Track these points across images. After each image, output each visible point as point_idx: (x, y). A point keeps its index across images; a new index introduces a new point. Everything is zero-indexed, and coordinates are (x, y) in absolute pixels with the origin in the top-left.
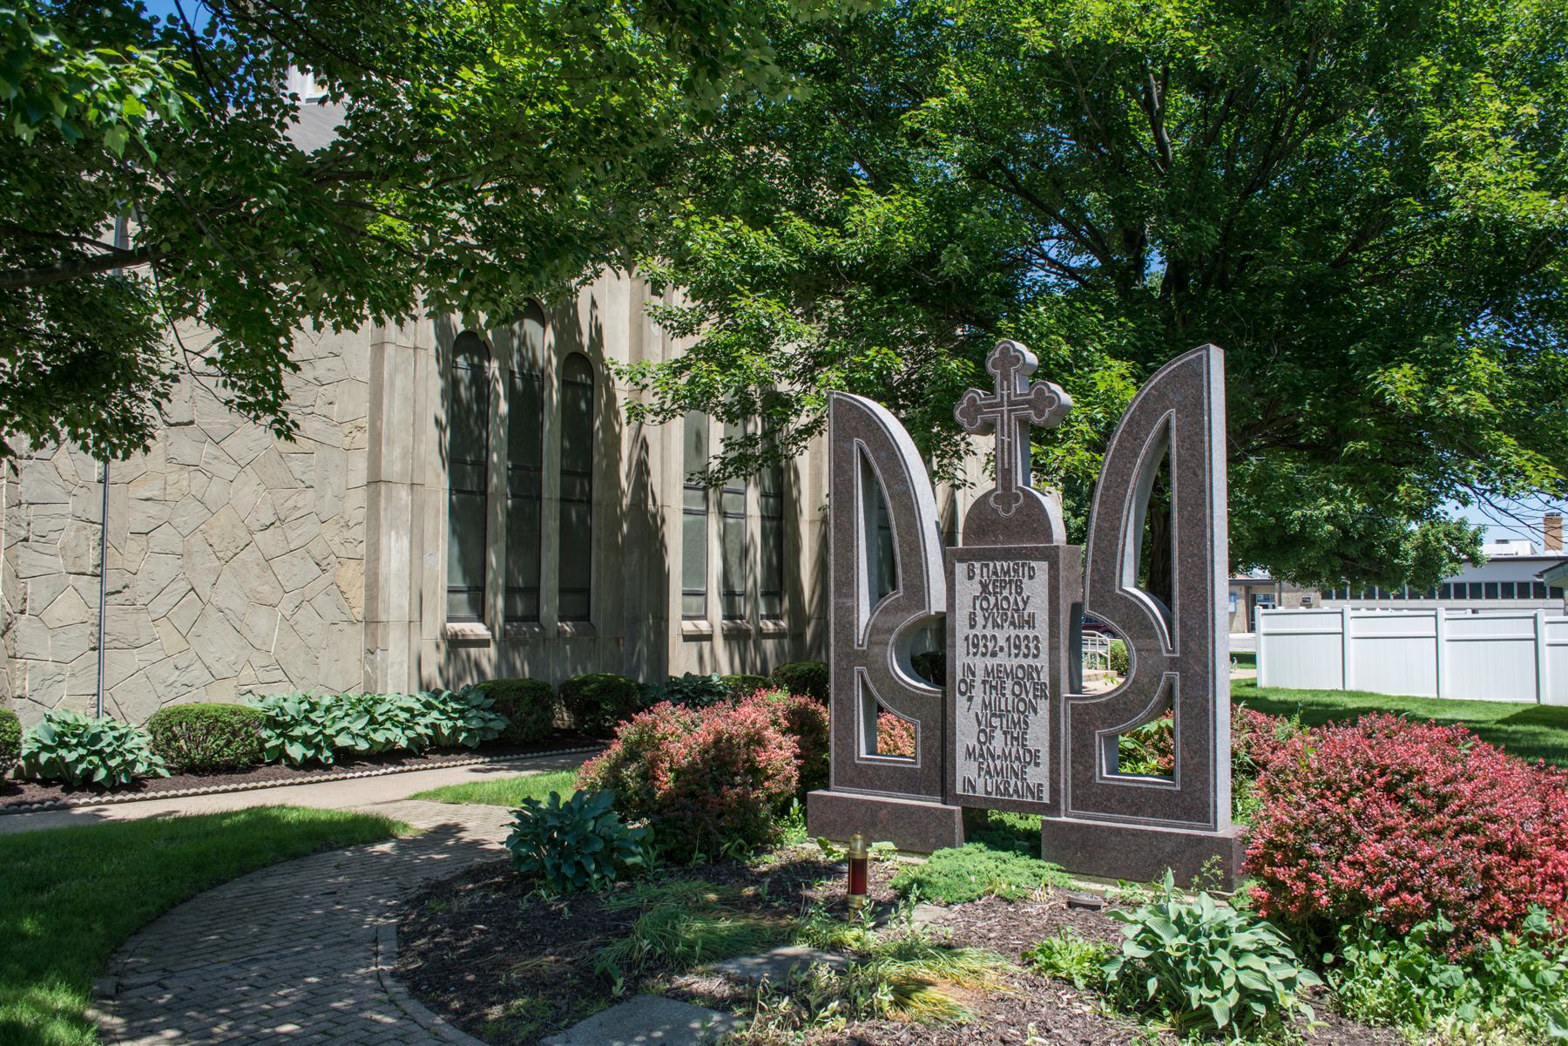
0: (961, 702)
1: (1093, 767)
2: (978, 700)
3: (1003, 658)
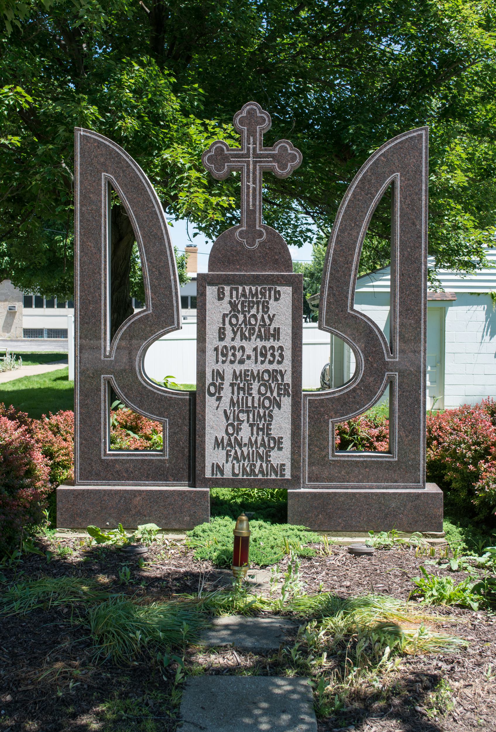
3: (250, 365)
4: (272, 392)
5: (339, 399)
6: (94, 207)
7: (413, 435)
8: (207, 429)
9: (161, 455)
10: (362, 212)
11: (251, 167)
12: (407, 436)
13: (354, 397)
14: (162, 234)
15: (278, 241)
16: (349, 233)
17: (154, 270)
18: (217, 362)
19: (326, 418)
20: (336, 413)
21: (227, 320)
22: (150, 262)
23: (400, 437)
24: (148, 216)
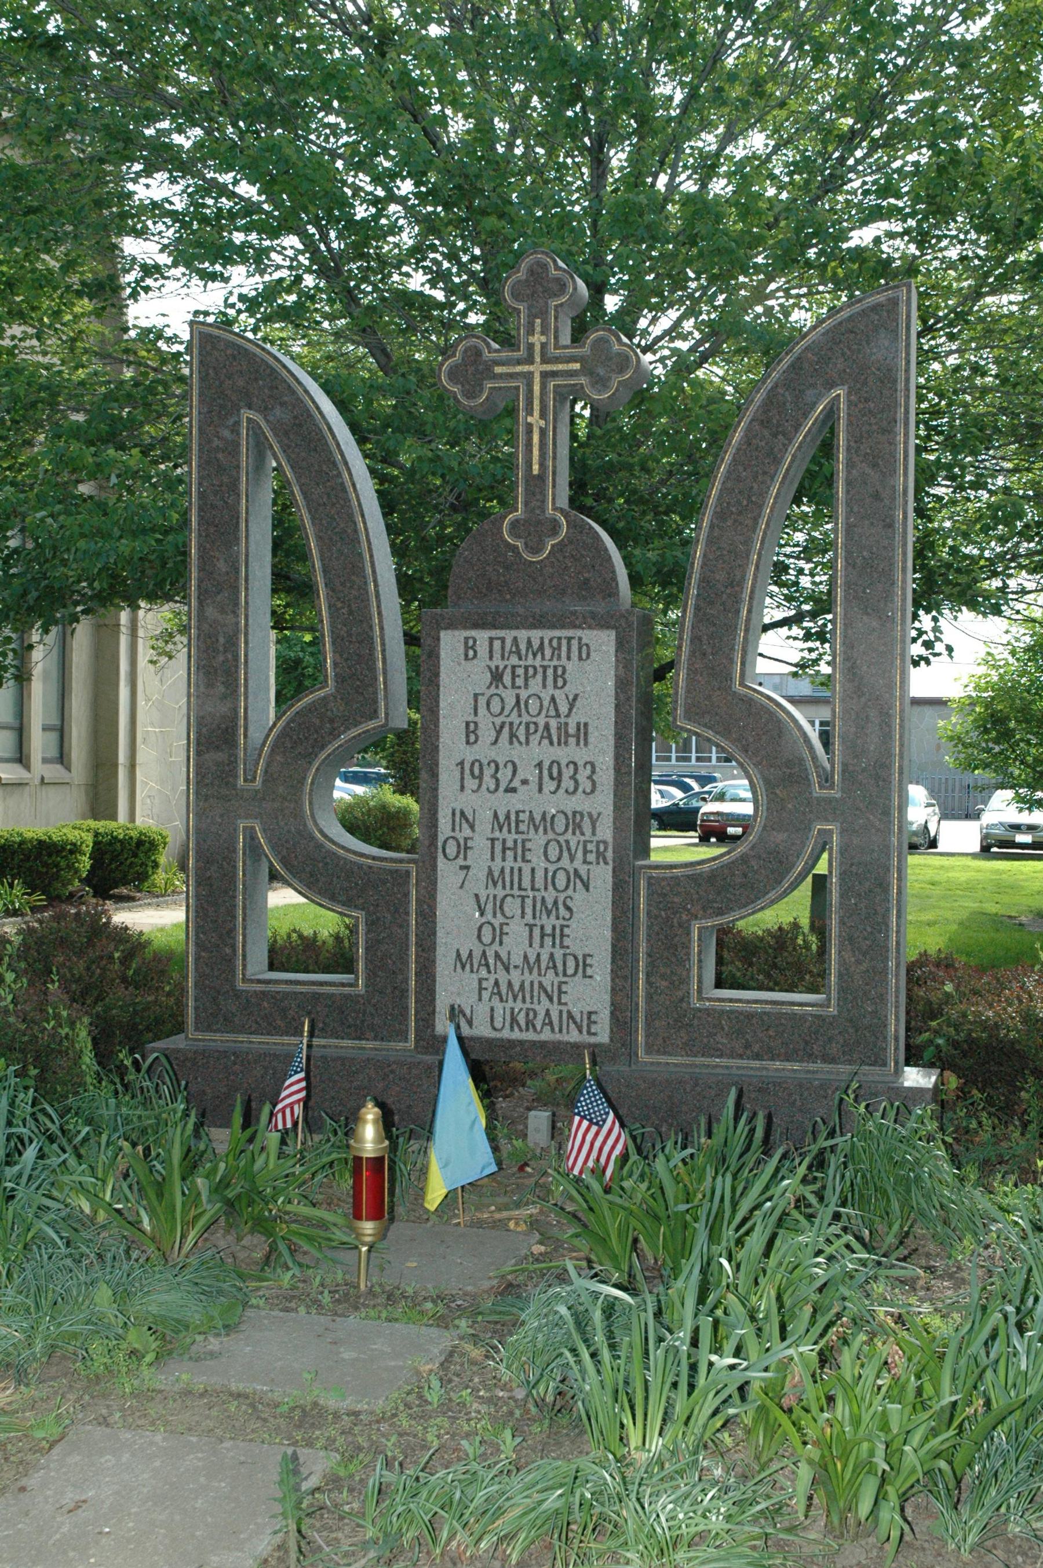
0: (447, 872)
1: (685, 981)
2: (479, 872)
3: (525, 800)
4: (572, 859)
5: (712, 877)
6: (225, 479)
7: (872, 959)
8: (440, 933)
9: (350, 985)
10: (765, 473)
11: (537, 388)
12: (858, 962)
13: (745, 876)
14: (356, 531)
15: (590, 541)
16: (735, 521)
17: (339, 605)
18: (462, 788)
19: (684, 917)
20: (704, 909)
21: (482, 701)
22: (333, 590)
23: (842, 962)
24: (328, 495)
